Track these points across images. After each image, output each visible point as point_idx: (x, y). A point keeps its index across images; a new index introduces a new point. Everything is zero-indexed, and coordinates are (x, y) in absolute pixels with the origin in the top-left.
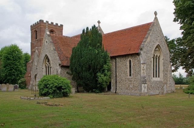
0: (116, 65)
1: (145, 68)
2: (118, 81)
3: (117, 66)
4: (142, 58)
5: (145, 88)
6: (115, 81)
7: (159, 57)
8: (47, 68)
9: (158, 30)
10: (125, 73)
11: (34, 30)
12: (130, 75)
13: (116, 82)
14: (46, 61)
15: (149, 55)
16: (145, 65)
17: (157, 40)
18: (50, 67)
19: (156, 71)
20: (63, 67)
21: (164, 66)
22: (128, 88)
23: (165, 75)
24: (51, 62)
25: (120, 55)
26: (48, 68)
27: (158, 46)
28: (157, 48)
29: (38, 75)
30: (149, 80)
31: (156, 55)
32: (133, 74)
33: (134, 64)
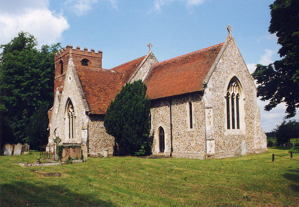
0: (171, 110)
1: (212, 114)
2: (174, 137)
3: (172, 113)
4: (208, 96)
5: (212, 146)
6: (170, 136)
7: (237, 97)
8: (71, 119)
9: (234, 54)
10: (184, 123)
11: (59, 60)
12: (191, 127)
13: (172, 137)
14: (69, 107)
15: (219, 94)
16: (212, 109)
17: (232, 69)
18: (75, 117)
19: (233, 119)
20: (93, 117)
21: (247, 109)
22: (189, 147)
23: (249, 125)
24: (76, 109)
25: (176, 94)
26: (72, 118)
27: (234, 80)
28: (233, 83)
29: (58, 130)
30: (220, 133)
31: (231, 93)
32: (195, 125)
33: (195, 108)
